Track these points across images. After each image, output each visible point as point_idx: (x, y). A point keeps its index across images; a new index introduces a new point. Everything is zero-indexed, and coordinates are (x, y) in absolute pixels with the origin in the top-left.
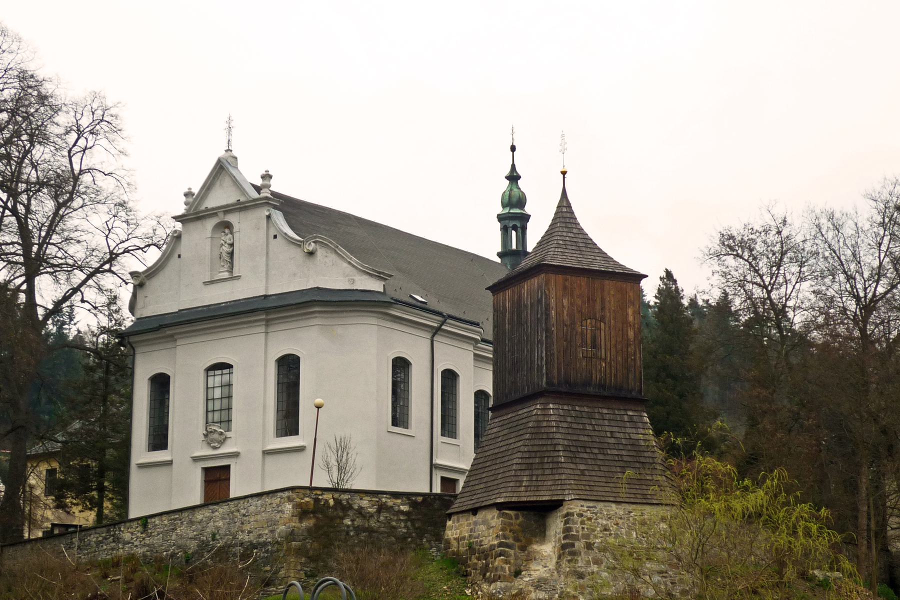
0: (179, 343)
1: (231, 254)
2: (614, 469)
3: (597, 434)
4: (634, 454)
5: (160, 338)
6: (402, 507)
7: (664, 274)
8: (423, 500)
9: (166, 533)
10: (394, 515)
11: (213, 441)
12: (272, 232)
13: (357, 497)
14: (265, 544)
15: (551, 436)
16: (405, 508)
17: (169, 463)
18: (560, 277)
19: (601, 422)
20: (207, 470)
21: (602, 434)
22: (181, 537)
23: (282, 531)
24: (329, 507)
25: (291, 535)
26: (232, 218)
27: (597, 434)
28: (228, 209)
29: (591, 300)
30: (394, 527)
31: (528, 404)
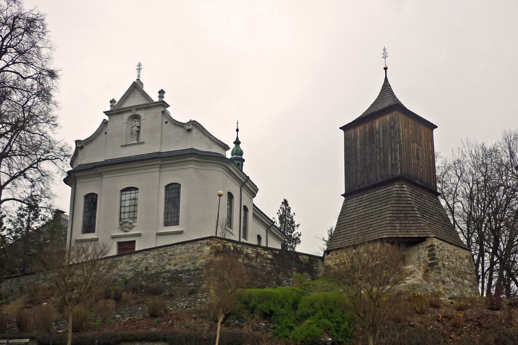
0: (104, 177)
1: (138, 132)
5: (93, 174)
6: (268, 256)
7: (283, 201)
8: (280, 254)
10: (264, 260)
11: (125, 227)
12: (165, 120)
14: (188, 270)
15: (409, 202)
16: (270, 256)
17: (97, 240)
20: (119, 244)
22: (121, 270)
23: (202, 263)
24: (231, 251)
26: (140, 113)
28: (138, 108)
30: (265, 267)
31: (369, 191)
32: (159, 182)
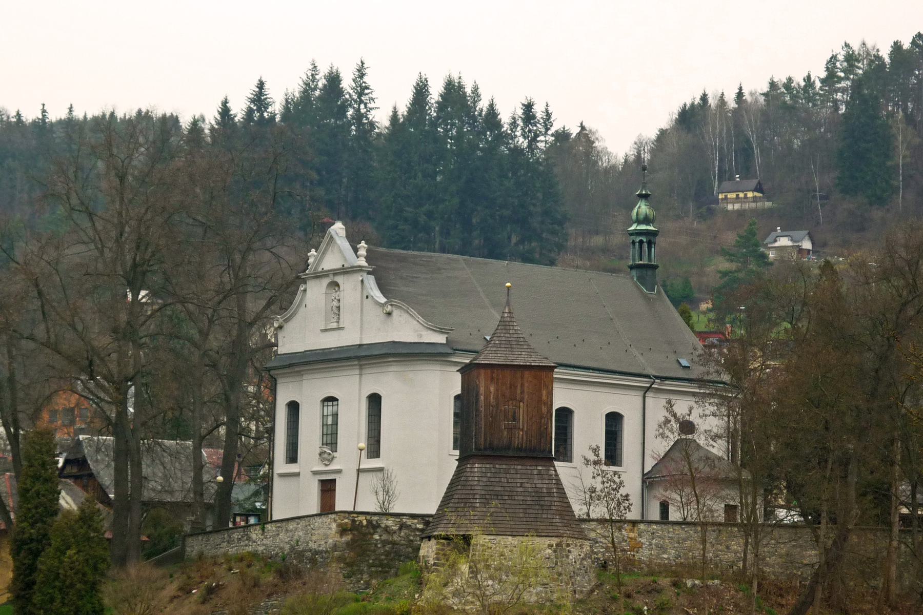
0: (305, 377)
1: (339, 308)
2: (517, 511)
3: (509, 485)
4: (537, 499)
9: (274, 536)
13: (384, 518)
14: (322, 552)
16: (420, 526)
18: (489, 371)
19: (515, 476)
20: (323, 482)
21: (514, 485)
24: (362, 526)
25: (335, 547)
26: (339, 279)
27: (509, 485)
29: (513, 386)
30: (412, 541)
32: (360, 390)
